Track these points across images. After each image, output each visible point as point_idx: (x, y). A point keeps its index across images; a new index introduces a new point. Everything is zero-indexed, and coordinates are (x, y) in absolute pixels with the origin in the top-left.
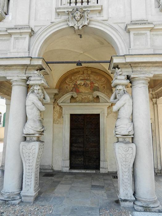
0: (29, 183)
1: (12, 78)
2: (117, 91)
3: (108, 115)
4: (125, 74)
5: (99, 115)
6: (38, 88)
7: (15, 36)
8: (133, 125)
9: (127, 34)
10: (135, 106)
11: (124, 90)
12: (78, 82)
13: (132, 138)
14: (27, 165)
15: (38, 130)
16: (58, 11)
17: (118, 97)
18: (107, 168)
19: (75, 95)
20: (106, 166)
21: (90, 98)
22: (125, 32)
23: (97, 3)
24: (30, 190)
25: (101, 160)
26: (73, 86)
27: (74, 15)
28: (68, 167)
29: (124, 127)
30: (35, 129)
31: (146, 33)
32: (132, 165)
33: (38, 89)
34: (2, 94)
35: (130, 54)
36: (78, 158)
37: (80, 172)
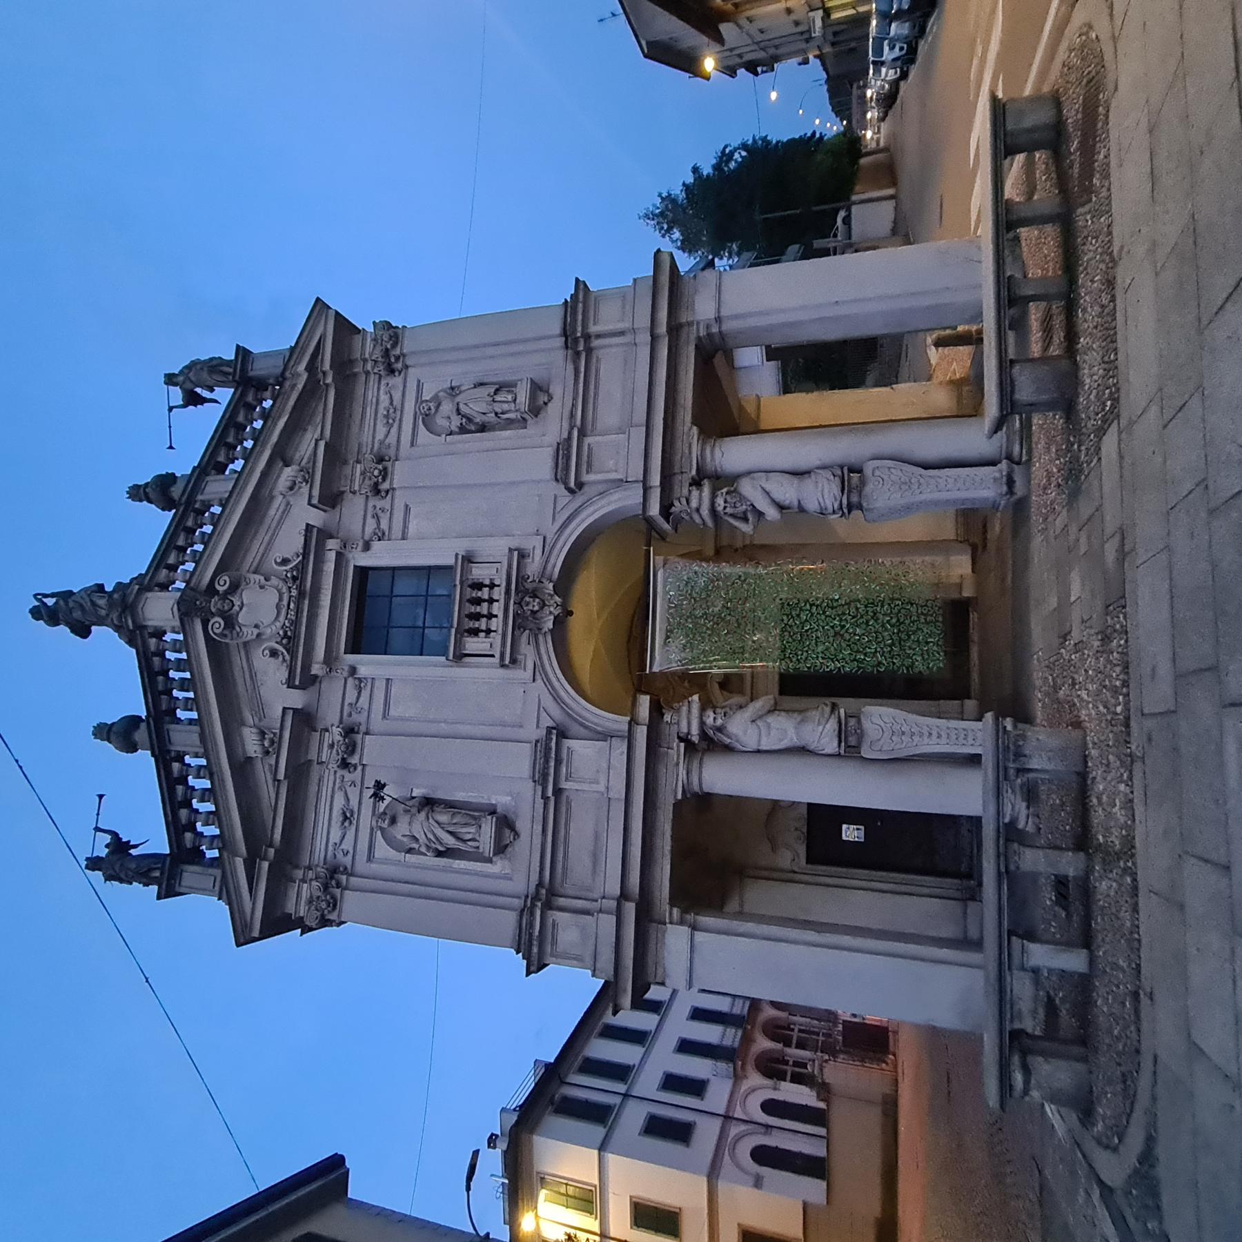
1: (680, 784)
2: (728, 510)
6: (710, 713)
9: (586, 488)
10: (768, 467)
13: (851, 470)
14: (926, 740)
15: (828, 709)
16: (507, 662)
26: (686, 684)
29: (822, 494)
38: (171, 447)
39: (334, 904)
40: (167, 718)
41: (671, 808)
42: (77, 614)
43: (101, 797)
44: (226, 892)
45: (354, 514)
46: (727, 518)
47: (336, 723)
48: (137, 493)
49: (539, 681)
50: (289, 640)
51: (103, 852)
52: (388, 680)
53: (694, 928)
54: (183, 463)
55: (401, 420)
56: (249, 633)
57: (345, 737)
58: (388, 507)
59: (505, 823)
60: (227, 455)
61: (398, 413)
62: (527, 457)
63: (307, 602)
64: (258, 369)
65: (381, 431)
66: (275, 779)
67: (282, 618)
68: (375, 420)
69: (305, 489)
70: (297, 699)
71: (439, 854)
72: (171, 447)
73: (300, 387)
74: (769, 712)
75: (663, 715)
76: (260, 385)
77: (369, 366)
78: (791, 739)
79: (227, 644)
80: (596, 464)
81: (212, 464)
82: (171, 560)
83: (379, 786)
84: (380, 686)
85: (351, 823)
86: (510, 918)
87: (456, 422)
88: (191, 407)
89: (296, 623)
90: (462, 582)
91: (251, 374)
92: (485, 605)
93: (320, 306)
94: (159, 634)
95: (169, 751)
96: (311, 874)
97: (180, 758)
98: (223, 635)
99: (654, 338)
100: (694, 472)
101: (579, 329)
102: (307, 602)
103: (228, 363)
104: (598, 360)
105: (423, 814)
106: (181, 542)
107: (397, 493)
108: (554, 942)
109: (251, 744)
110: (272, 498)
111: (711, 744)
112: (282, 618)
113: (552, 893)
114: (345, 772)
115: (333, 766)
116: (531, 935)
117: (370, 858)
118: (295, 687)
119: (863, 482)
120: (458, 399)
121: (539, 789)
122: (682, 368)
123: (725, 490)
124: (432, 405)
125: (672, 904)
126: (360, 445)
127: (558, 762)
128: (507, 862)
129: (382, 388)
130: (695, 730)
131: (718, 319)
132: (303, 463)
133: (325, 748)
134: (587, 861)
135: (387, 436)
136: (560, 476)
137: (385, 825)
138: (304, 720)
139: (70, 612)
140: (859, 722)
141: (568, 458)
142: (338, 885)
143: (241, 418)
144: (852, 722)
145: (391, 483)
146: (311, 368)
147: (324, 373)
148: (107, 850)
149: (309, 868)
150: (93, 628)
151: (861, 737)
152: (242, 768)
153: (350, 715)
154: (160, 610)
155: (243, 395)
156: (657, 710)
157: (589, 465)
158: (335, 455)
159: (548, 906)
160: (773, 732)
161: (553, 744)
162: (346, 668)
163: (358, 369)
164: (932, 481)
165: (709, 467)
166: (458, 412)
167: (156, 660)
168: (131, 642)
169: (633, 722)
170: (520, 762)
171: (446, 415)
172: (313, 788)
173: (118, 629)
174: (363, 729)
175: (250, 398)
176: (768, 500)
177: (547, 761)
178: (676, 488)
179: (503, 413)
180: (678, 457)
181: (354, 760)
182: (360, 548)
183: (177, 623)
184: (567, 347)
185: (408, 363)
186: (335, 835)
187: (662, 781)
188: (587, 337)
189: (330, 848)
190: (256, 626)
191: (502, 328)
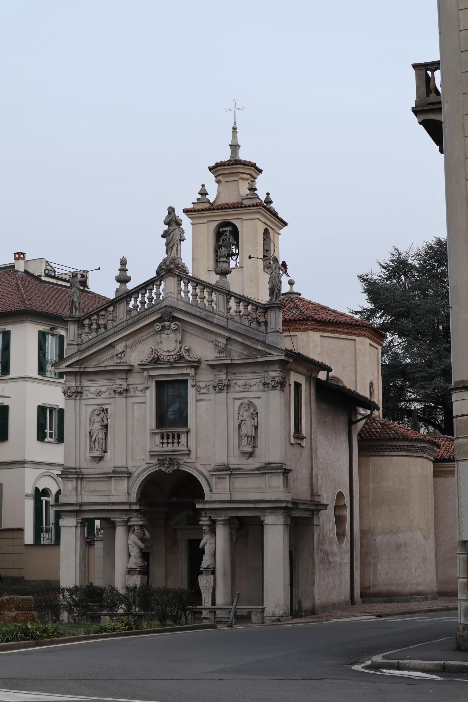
4: (208, 515)
7: (116, 479)
15: (139, 565)
32: (211, 592)
39: (70, 397)
43: (99, 269)
45: (206, 377)
49: (145, 466)
53: (76, 526)
55: (244, 392)
61: (247, 390)
65: (240, 383)
68: (246, 379)
71: (90, 433)
78: (132, 554)
80: (218, 480)
92: (172, 441)
95: (116, 304)
105: (100, 427)
108: (67, 481)
109: (120, 347)
111: (129, 529)
113: (81, 478)
117: (87, 405)
127: (120, 477)
130: (132, 523)
134: (93, 488)
140: (137, 574)
142: (76, 396)
144: (137, 572)
149: (81, 382)
151: (132, 575)
156: (136, 511)
157: (220, 478)
159: (77, 478)
160: (132, 549)
169: (130, 504)
174: (128, 395)
181: (117, 395)
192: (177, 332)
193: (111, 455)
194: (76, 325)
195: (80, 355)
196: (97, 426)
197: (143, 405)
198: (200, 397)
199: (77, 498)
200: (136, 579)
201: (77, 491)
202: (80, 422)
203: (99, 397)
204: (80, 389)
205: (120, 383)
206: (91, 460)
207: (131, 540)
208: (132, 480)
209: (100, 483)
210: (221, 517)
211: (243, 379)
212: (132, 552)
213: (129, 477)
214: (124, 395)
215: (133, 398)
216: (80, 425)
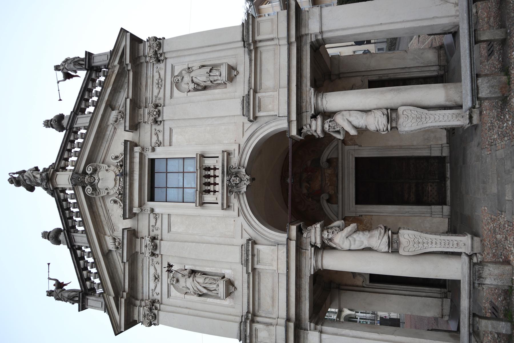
0: (455, 243)
1: (312, 267)
2: (330, 130)
3: (357, 145)
4: (309, 121)
5: (357, 159)
6: (325, 232)
7: (256, 262)
8: (375, 109)
9: (258, 119)
10: (350, 108)
11: (330, 122)
12: (305, 191)
14: (430, 246)
15: (383, 231)
16: (225, 207)
17: (338, 129)
18: (442, 144)
19: (324, 197)
20: (439, 148)
21: (330, 173)
22: (255, 122)
23: (218, 157)
24: (463, 243)
25: (429, 155)
26: (310, 199)
27: (234, 185)
28: (442, 208)
30: (382, 234)
31: (259, 98)
32: (425, 111)
33: (328, 232)
34: (324, 306)
35: (286, 114)
36: (428, 191)
37: (449, 187)
38: (60, 100)
39: (155, 317)
40: (72, 230)
41: (308, 278)
42: (28, 182)
43: (49, 264)
44: (107, 309)
45: (146, 135)
46: (332, 134)
47: (147, 235)
48: (48, 124)
49: (241, 217)
50: (122, 194)
51: (53, 288)
52: (169, 214)
53: (321, 332)
54: (67, 109)
55: (165, 85)
56: (104, 193)
57: (152, 242)
58: (161, 129)
59: (230, 283)
60: (86, 104)
61: (163, 82)
62: (228, 101)
63: (128, 178)
64: (96, 62)
66: (122, 262)
67: (117, 185)
69: (122, 121)
70: (128, 223)
71: (200, 296)
72: (60, 100)
73: (116, 72)
74: (355, 232)
75: (302, 234)
76: (98, 69)
77: (148, 59)
78: (366, 244)
79: (94, 198)
81: (79, 110)
82: (66, 156)
83: (170, 266)
84: (165, 218)
85: (158, 280)
86: (236, 326)
87: (192, 86)
88: (67, 80)
89: (124, 188)
90: (200, 168)
91: (93, 65)
93: (123, 31)
94: (63, 190)
95: (75, 245)
96: (143, 303)
97: (80, 248)
98: (92, 194)
99: (289, 44)
100: (313, 112)
101: (251, 39)
102: (128, 178)
103: (82, 60)
104: (261, 53)
105: (191, 278)
106: (69, 147)
107: (166, 123)
108: (256, 337)
109: (111, 245)
110: (108, 126)
111: (326, 246)
112: (117, 185)
113: (254, 315)
114: (153, 258)
115: (148, 255)
116: (246, 335)
117: (169, 295)
118: (127, 219)
119: (398, 117)
120: (192, 74)
121: (245, 268)
122: (304, 57)
123: (329, 120)
124: (179, 78)
125: (310, 322)
126: (146, 99)
127: (253, 255)
128: (232, 300)
129: (155, 69)
131: (321, 32)
132: (120, 109)
133: (143, 247)
135: (158, 94)
136: (245, 112)
137: (174, 283)
138: (133, 234)
139: (23, 180)
140: (398, 237)
141: (249, 104)
143: (90, 86)
144: (395, 236)
145: (162, 118)
146: (121, 62)
147: (127, 65)
148: (55, 287)
149: (142, 300)
150: (36, 187)
151: (399, 244)
152: (107, 254)
153: (153, 231)
154: (63, 180)
155: (90, 75)
156: (300, 231)
157: (260, 107)
158: (136, 104)
159: (253, 321)
160: (357, 242)
161: (250, 248)
162: (149, 209)
163: (143, 60)
164: (431, 116)
165: (321, 108)
166: (193, 81)
167: (64, 203)
168: (53, 195)
169: (289, 239)
170: (235, 255)
171: (186, 83)
172: (140, 264)
173: (46, 189)
174: (159, 238)
175: (93, 76)
176: (351, 126)
177: (248, 256)
178: (304, 119)
179: (214, 81)
180: (304, 104)
181: (157, 252)
182: (150, 150)
183: (71, 186)
184: (245, 47)
185: (166, 56)
186: (152, 286)
187: (303, 265)
188: (255, 42)
189: (151, 291)
190: (107, 189)
191: (212, 39)
192: (99, 169)
193: (227, 269)
194: (88, 297)
195: (109, 295)
196: (189, 283)
197: (172, 219)
198: (167, 142)
199: (280, 325)
200: (406, 236)
201: (271, 324)
202: (186, 308)
203: (160, 277)
204: (148, 302)
205: (144, 246)
206: (233, 298)
207: (343, 242)
208: (259, 239)
209: (262, 288)
210: (310, 99)
211: (152, 88)
212: (362, 242)
213: (254, 243)
214: (158, 242)
215: (163, 231)
216: (190, 308)
